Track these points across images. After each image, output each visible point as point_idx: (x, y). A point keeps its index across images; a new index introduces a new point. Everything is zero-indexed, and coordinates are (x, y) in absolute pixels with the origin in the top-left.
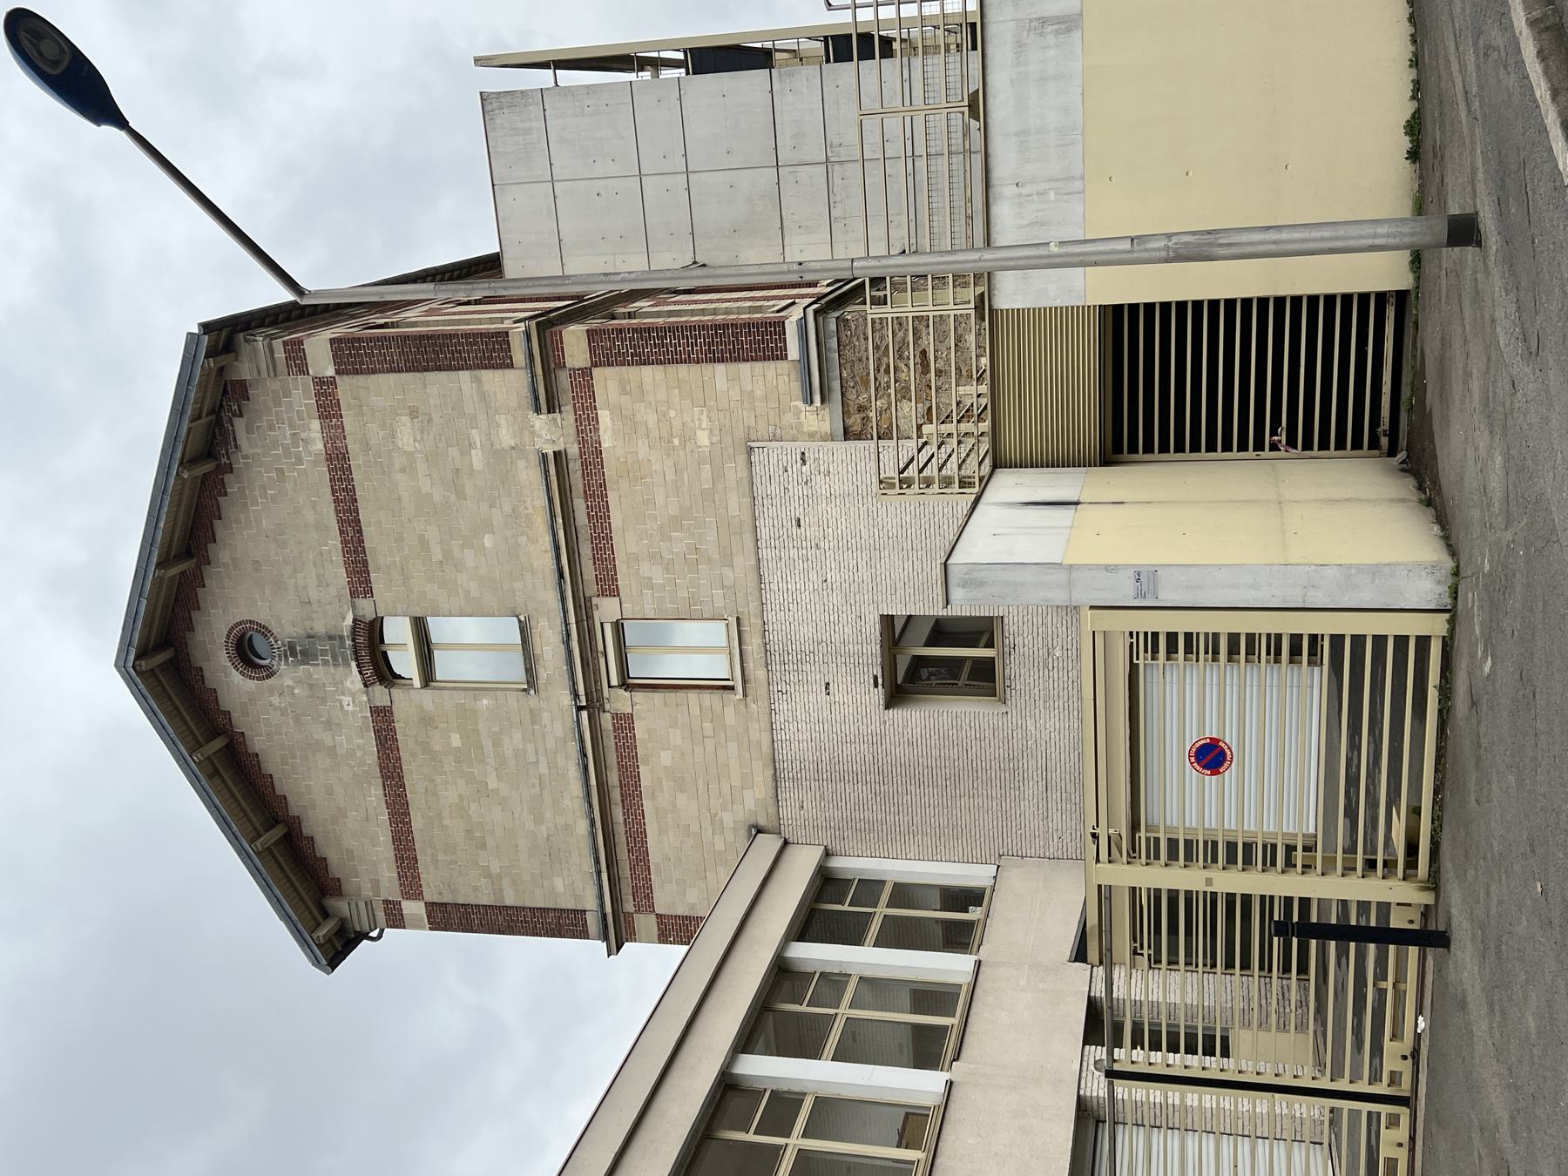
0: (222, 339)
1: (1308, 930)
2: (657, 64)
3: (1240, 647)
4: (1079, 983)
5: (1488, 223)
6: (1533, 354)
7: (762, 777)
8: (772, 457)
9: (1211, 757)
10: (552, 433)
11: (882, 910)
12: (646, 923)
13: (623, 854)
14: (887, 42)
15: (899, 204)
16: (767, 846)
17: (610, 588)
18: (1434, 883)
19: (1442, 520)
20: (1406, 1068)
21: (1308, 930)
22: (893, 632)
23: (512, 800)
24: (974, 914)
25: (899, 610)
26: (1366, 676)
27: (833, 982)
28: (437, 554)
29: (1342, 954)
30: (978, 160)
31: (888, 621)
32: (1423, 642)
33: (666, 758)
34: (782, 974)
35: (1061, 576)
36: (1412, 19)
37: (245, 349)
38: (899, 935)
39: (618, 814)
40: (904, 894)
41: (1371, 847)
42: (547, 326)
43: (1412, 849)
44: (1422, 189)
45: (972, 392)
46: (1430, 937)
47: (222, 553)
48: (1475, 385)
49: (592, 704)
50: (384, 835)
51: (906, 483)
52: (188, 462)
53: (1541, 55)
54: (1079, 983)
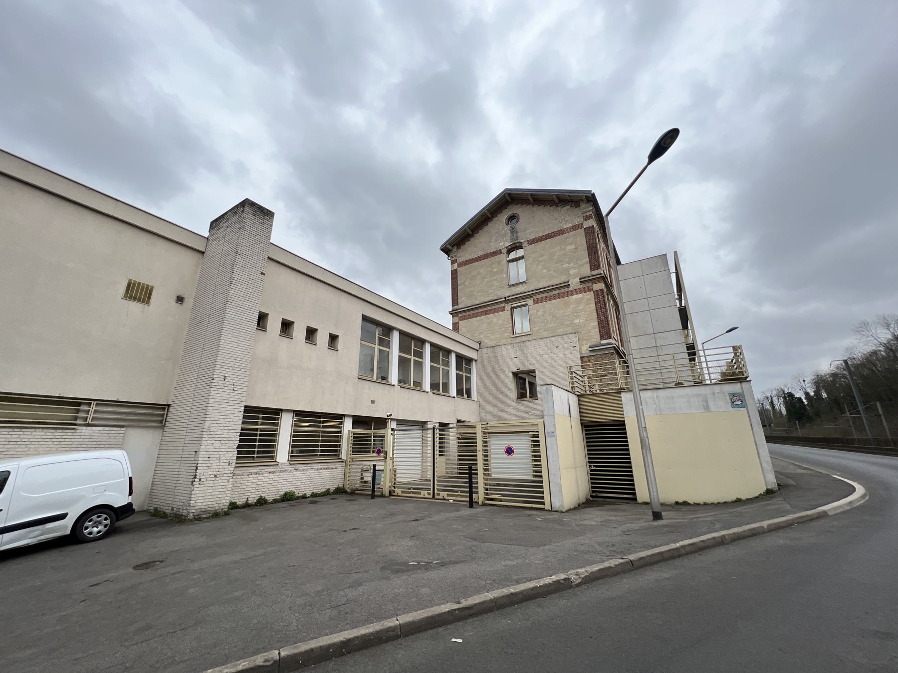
0: (590, 199)
1: (470, 474)
2: (680, 299)
3: (537, 458)
4: (452, 421)
5: (660, 522)
6: (624, 532)
7: (493, 343)
8: (574, 339)
9: (509, 451)
10: (575, 283)
11: (464, 374)
12: (457, 320)
13: (472, 312)
14: (694, 360)
15: (647, 366)
16: (476, 346)
17: (536, 302)
18: (484, 505)
19: (575, 509)
20: (441, 497)
21: (470, 474)
22: (531, 373)
23: (482, 286)
24: (465, 396)
25: (537, 374)
26: (531, 491)
27: (447, 364)
28: (540, 259)
29: (465, 483)
30: (662, 386)
31: (534, 371)
32: (543, 503)
33: (495, 320)
34: (448, 352)
35: (551, 413)
36: (719, 503)
37: (589, 205)
38: (459, 378)
39: (481, 310)
40: (468, 379)
41: (491, 490)
42: (603, 279)
43: (492, 499)
44: (668, 505)
45: (597, 389)
46: (472, 504)
47: (535, 208)
48: (613, 518)
49: (506, 301)
50: (472, 257)
51: (571, 373)
52: (558, 196)
53: (714, 538)
54: (452, 421)
